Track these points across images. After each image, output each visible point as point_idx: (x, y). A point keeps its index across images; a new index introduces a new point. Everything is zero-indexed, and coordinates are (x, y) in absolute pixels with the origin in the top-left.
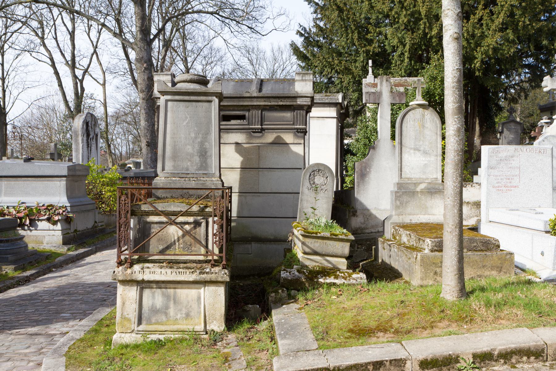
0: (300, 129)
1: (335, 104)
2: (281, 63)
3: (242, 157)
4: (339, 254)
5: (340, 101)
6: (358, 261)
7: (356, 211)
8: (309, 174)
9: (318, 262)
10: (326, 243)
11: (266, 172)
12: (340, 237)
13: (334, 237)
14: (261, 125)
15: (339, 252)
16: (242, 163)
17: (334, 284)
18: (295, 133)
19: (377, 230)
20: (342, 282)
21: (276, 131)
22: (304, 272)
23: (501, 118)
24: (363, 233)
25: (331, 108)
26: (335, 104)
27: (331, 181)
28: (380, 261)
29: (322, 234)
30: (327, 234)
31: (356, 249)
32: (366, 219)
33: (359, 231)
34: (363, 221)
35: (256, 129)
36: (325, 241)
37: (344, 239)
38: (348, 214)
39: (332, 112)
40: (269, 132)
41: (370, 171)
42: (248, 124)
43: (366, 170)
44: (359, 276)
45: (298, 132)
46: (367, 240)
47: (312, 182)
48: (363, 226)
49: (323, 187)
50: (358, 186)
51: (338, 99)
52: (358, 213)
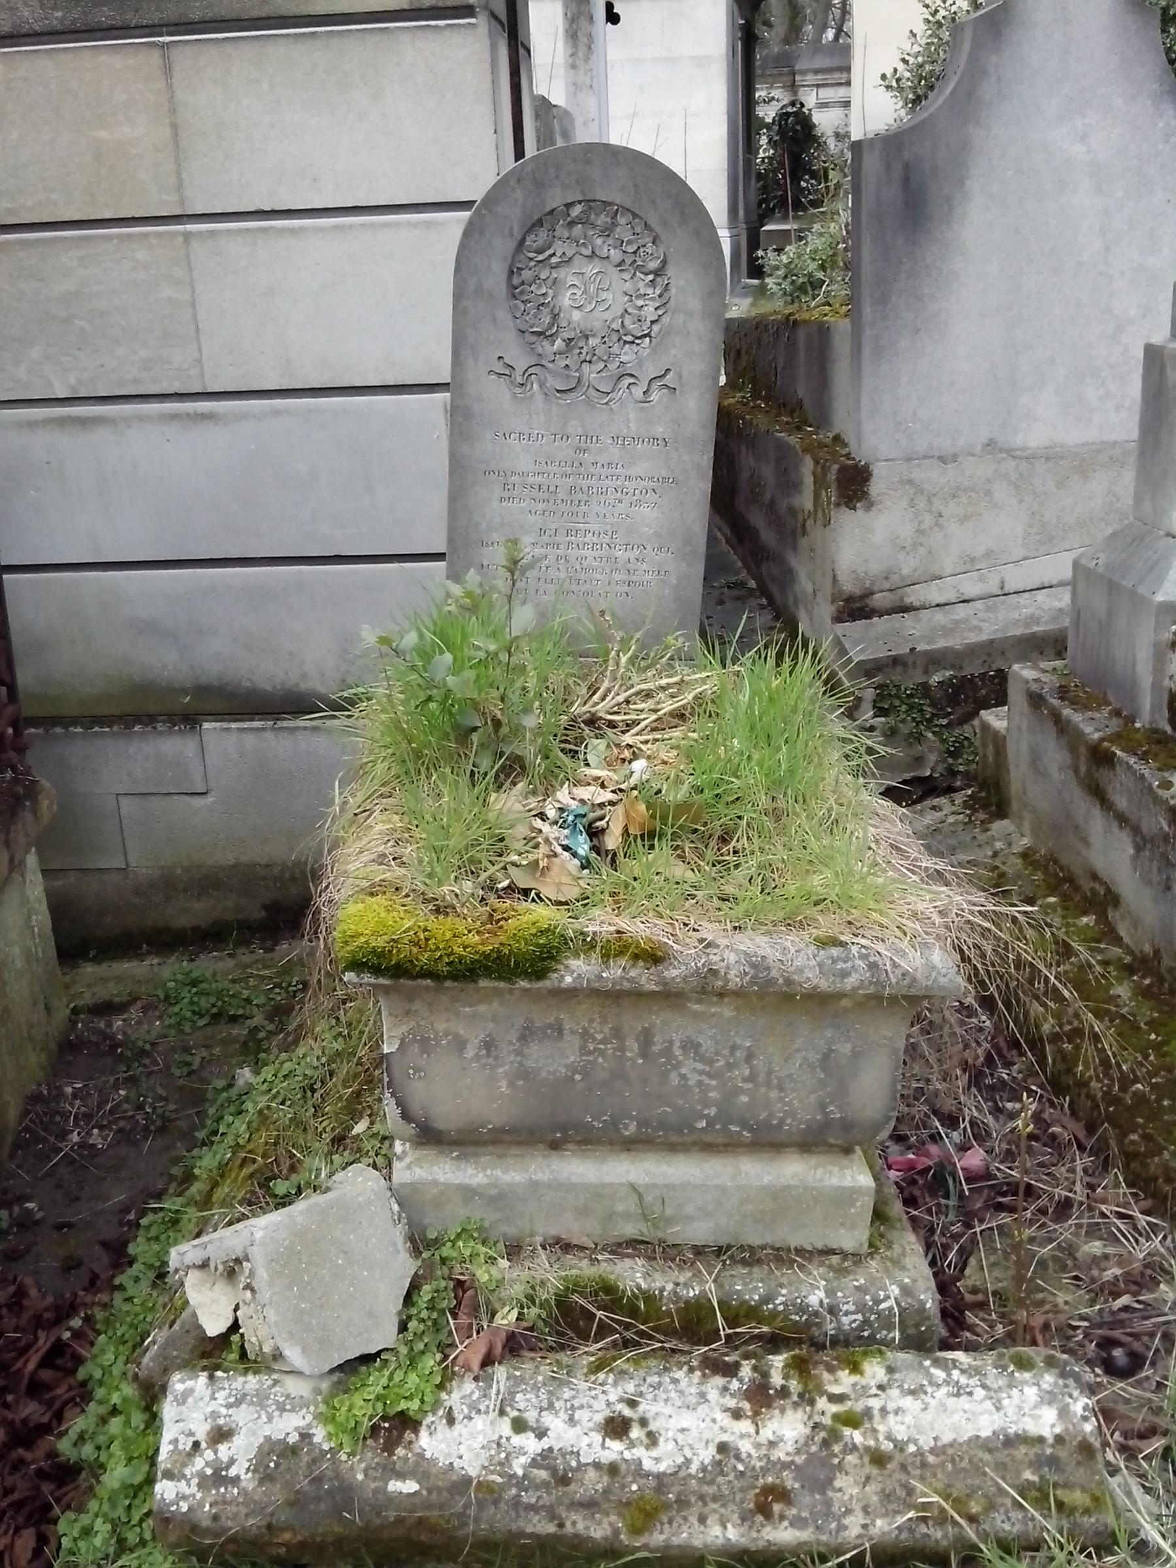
32: (928, 520)
48: (908, 566)
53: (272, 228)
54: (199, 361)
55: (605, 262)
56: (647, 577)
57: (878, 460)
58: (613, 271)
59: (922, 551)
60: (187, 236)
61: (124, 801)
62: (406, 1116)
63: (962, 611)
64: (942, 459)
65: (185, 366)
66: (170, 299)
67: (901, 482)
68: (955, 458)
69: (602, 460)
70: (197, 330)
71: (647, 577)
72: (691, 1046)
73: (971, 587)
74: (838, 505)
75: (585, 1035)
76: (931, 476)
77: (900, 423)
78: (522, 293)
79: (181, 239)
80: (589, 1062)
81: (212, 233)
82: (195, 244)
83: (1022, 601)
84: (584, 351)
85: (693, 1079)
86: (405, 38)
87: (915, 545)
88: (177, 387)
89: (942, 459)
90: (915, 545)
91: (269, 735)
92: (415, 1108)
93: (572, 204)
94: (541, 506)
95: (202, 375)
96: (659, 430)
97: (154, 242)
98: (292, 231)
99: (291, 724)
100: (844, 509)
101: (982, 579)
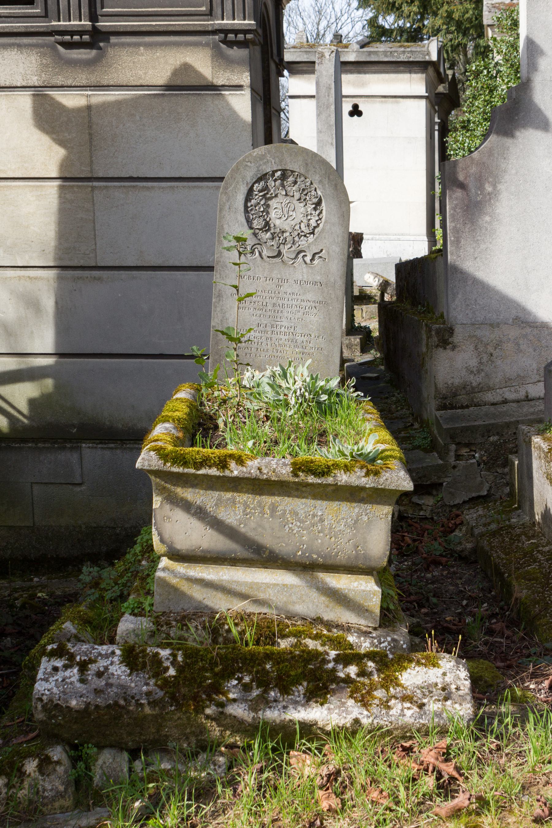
0: (236, 32)
1: (422, 66)
2: (333, 20)
3: (61, 143)
4: (341, 559)
5: (434, 57)
6: (458, 501)
7: (451, 331)
8: (243, 191)
9: (243, 596)
10: (274, 508)
11: (117, 192)
12: (343, 478)
13: (311, 479)
14: (93, 18)
15: (343, 548)
16: (64, 164)
17: (308, 730)
18: (215, 47)
19: (521, 395)
20: (347, 721)
21: (148, 39)
22: (156, 660)
23: (43, 587)
24: (477, 405)
25: (414, 76)
26: (422, 66)
27: (335, 219)
28: (538, 510)
29: (252, 467)
30: (279, 466)
31: (452, 460)
32: (485, 358)
33: (463, 399)
34: (473, 363)
35: (72, 33)
36: (268, 500)
37: (362, 489)
38: (424, 337)
39: (416, 84)
40: (123, 45)
41: (495, 194)
42: (46, 15)
43: (481, 187)
44: (432, 675)
45: (230, 44)
46: (488, 430)
47: (258, 223)
48: (475, 380)
49: (303, 243)
50: (457, 241)
51: (428, 54)
52: (458, 336)
53: (137, 186)
54: (95, 250)
55: (292, 198)
56: (313, 351)
57: (457, 324)
58: (295, 202)
59: (483, 374)
60: (93, 188)
61: (36, 488)
62: (162, 541)
63: (505, 408)
64: (491, 325)
65: (87, 252)
66: (82, 219)
67: (469, 336)
68: (498, 325)
69: (289, 291)
70: (95, 235)
71: (313, 351)
72: (295, 513)
73: (510, 395)
74: (437, 346)
75: (246, 506)
76: (485, 333)
77: (468, 305)
78: (251, 210)
79: (90, 189)
80: (247, 518)
81: (106, 187)
82: (96, 192)
83: (537, 403)
84: (281, 238)
85: (296, 530)
86: (209, 99)
87: (479, 371)
88: (82, 263)
89: (491, 325)
90: (479, 371)
91: (118, 451)
92: (166, 536)
93: (277, 171)
94: (259, 312)
95: (96, 257)
96: (318, 278)
97: (76, 189)
98: (148, 188)
99: (131, 446)
100: (441, 350)
101: (516, 391)
